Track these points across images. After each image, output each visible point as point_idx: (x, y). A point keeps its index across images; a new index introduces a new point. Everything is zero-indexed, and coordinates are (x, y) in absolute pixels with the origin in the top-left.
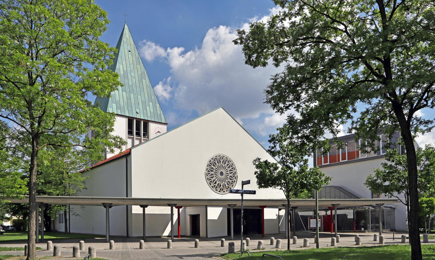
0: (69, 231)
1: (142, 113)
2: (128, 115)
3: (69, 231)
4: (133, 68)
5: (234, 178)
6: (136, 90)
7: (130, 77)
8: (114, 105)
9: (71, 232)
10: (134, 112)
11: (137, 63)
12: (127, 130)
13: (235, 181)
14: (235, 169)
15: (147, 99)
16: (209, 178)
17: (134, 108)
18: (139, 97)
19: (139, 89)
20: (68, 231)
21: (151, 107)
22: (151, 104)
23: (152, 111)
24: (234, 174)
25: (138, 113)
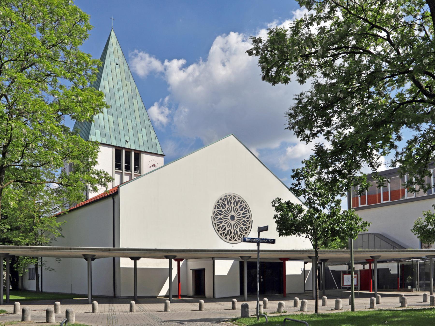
0: (42, 290)
1: (132, 141)
2: (115, 145)
3: (42, 290)
4: (121, 86)
5: (248, 223)
6: (125, 112)
7: (117, 97)
8: (98, 132)
9: (44, 291)
10: (123, 140)
11: (127, 79)
12: (114, 163)
13: (249, 227)
14: (249, 212)
15: (139, 124)
16: (247, 213)
17: (122, 135)
18: (129, 122)
19: (129, 112)
20: (40, 290)
21: (145, 134)
22: (144, 130)
23: (145, 139)
24: (248, 218)
25: (128, 142)
